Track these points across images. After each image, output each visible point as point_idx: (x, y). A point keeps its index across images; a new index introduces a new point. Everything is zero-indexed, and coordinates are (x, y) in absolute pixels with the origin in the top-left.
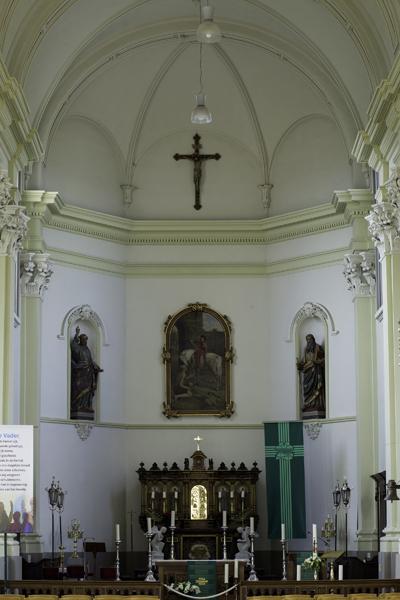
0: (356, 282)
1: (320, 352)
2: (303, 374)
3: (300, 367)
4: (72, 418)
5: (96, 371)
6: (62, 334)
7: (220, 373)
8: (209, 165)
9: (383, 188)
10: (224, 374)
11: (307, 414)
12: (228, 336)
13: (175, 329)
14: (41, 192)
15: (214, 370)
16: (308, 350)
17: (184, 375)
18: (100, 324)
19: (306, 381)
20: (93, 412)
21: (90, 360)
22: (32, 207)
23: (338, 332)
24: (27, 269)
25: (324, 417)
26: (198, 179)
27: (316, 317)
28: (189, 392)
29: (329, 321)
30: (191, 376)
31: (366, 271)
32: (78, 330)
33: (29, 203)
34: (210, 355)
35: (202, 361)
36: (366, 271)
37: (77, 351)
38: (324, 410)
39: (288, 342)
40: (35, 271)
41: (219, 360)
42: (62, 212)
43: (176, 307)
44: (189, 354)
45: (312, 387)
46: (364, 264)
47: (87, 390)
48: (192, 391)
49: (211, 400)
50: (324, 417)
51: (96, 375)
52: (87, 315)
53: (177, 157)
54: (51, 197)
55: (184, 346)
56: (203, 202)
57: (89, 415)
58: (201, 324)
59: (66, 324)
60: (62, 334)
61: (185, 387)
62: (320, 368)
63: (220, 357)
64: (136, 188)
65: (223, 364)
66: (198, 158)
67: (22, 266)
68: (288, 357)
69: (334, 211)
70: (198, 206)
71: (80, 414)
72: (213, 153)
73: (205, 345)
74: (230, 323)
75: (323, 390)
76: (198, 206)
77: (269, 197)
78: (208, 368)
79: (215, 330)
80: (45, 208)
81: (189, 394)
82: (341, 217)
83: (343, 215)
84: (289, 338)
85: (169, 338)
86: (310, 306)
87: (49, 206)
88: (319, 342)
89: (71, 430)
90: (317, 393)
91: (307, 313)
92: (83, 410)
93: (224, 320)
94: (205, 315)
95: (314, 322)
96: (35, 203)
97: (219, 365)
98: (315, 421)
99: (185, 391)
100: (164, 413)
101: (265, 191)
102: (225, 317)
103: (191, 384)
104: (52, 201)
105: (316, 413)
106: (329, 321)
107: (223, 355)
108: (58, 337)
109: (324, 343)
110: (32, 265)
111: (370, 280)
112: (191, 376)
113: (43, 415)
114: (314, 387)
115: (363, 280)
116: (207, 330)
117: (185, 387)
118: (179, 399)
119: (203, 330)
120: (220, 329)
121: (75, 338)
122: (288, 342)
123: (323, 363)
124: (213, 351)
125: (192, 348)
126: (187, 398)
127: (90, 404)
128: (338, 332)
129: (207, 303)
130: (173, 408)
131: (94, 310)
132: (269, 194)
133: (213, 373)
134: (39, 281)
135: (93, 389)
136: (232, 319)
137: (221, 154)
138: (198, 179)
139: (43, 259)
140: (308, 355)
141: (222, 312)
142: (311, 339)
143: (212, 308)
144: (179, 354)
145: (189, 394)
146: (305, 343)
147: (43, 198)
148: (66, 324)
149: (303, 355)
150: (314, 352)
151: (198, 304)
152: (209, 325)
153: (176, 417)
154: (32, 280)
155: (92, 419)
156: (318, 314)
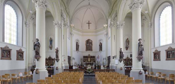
1: (102, 44)
3: (99, 45)
5: (79, 46)
34: (90, 44)
40: (72, 34)
43: (87, 39)
44: (88, 44)
62: (102, 45)
66: (89, 23)
78: (90, 46)
82: (104, 29)
89: (76, 52)
93: (92, 41)
113: (73, 50)
134: (72, 35)
142: (100, 42)
152: (90, 41)
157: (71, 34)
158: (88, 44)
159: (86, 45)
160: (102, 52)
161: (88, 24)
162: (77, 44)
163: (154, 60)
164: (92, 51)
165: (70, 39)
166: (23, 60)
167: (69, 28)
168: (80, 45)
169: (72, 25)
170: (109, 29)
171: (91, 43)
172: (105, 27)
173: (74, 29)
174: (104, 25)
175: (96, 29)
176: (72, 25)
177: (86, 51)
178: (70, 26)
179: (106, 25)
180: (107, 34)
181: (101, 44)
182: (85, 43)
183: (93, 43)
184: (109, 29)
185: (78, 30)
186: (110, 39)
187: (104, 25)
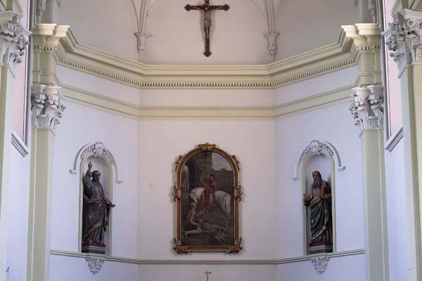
0: (364, 115)
1: (328, 189)
2: (309, 210)
3: (307, 202)
4: (82, 252)
5: (109, 206)
6: (75, 169)
7: (229, 210)
8: (218, 16)
9: (388, 44)
10: (232, 211)
11: (313, 248)
12: (236, 175)
13: (186, 168)
14: (52, 26)
15: (223, 208)
16: (314, 186)
17: (194, 212)
18: (113, 161)
19: (313, 216)
20: (104, 246)
21: (102, 194)
22: (45, 40)
23: (344, 168)
24: (38, 101)
25: (332, 251)
26: (207, 29)
27: (322, 155)
28: (198, 228)
29: (335, 157)
30: (201, 213)
31: (374, 104)
32: (90, 166)
33: (41, 36)
34: (219, 193)
35: (211, 200)
36: (374, 104)
37: (89, 186)
38: (330, 192)
39: (295, 179)
40: (46, 104)
41: (228, 198)
42: (76, 51)
43: (186, 146)
44: (199, 192)
45: (319, 222)
46: (372, 97)
47: (99, 224)
48: (202, 227)
49: (220, 236)
50: (332, 251)
51: (108, 210)
52: (101, 152)
53: (188, 8)
54: (63, 31)
55: (193, 185)
56: (212, 49)
57: (101, 249)
58: (210, 163)
59: (79, 160)
60: (75, 169)
61: (195, 224)
62: (327, 202)
63: (229, 195)
64: (150, 36)
65: (232, 202)
66: (207, 8)
67: (33, 98)
68: (295, 196)
69: (340, 50)
70: (207, 53)
71: (91, 247)
72: (222, 4)
73: (214, 183)
74: (238, 162)
75: (330, 225)
76: (207, 53)
77: (275, 45)
78: (217, 206)
79: (224, 169)
80: (56, 43)
81: (199, 230)
82: (347, 56)
83: (349, 54)
84: (295, 176)
85: (180, 175)
86: (316, 144)
87: (62, 40)
88: (325, 178)
89: (81, 263)
90: (324, 228)
91: (314, 150)
92: (95, 243)
93: (232, 160)
94: (214, 155)
95: (320, 159)
96: (48, 37)
97: (228, 202)
98: (322, 255)
99: (195, 228)
100: (175, 249)
101: (272, 39)
102: (234, 157)
103: (201, 221)
104: (63, 35)
105: (323, 247)
106: (335, 157)
107: (231, 193)
108: (70, 171)
109: (330, 180)
110: (43, 97)
111: (377, 113)
112: (201, 213)
113: (52, 248)
114: (320, 222)
115: (371, 113)
116: (216, 170)
117: (195, 224)
118: (189, 235)
119: (212, 170)
120: (229, 168)
121: (88, 173)
122: (295, 179)
123: (330, 198)
124: (222, 189)
125: (202, 186)
126: (198, 234)
127: (101, 238)
128: (344, 168)
129: (215, 143)
130: (183, 244)
131: (108, 148)
132: (276, 43)
133: (222, 211)
134: (51, 114)
135: (105, 224)
136: (240, 158)
137: (229, 4)
138: (207, 29)
139: (54, 91)
140: (314, 191)
141: (231, 152)
142: (317, 175)
143: (221, 148)
144: (190, 192)
145: (199, 230)
146: (312, 180)
147: (54, 32)
148: (79, 160)
149: (309, 192)
150: (320, 188)
151: (207, 145)
152: (218, 164)
153: (186, 253)
154: (43, 111)
155: (103, 253)
156: (324, 151)
157: (37, 102)
158: (199, 192)
159: (176, 198)
160: (334, 263)
161: (197, 14)
162: (87, 192)
163: (237, 250)
164: (237, 250)
165: (24, 153)
166: (307, 254)
167: (24, 58)
168: (121, 195)
169: (47, 29)
170: (393, 69)
171: (229, 181)
172: (357, 43)
173: (68, 56)
174: (349, 30)
175: (274, 53)
176: (47, 29)
177: (179, 250)
178: (36, 36)
179: (365, 29)
180: (377, 103)
181: (318, 193)
182: (166, 180)
183: (248, 180)
184: (393, 69)
185: (106, 69)
186: (402, 148)
187: (349, 30)
